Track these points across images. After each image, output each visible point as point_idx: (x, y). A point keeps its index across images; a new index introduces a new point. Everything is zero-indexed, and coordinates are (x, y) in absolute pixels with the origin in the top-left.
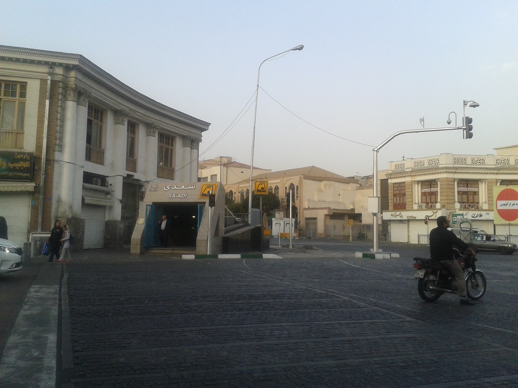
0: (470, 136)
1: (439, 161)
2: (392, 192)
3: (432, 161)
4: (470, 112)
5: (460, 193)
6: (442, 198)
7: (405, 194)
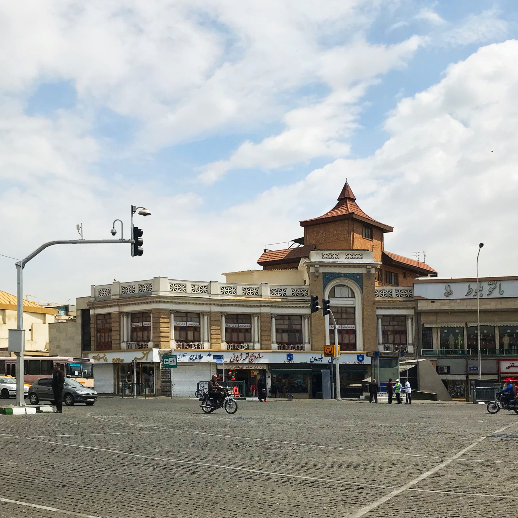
0: (138, 252)
1: (151, 286)
2: (95, 327)
3: (144, 286)
4: (140, 222)
5: (229, 330)
6: (155, 335)
7: (111, 329)
